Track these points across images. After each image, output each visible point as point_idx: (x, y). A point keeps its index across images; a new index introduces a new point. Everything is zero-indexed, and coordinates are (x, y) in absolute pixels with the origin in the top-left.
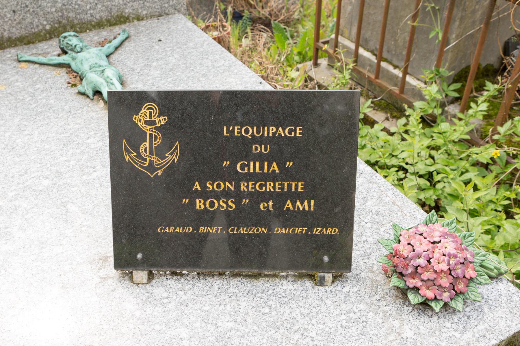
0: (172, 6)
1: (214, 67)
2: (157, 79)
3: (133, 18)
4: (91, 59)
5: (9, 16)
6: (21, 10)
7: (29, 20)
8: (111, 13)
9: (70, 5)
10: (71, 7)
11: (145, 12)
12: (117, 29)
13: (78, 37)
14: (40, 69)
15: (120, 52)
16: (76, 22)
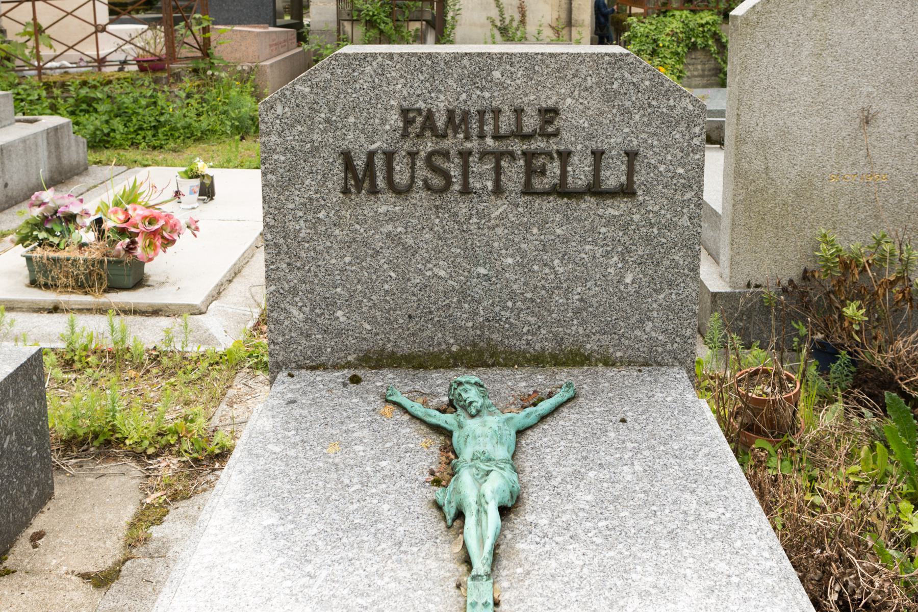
0: (669, 352)
1: (698, 517)
2: (581, 514)
3: (597, 360)
4: (481, 439)
5: (401, 321)
6: (421, 317)
7: (428, 333)
8: (560, 345)
9: (497, 322)
10: (497, 325)
11: (619, 354)
12: (563, 375)
13: (482, 386)
14: (408, 426)
15: (546, 427)
16: (501, 348)
